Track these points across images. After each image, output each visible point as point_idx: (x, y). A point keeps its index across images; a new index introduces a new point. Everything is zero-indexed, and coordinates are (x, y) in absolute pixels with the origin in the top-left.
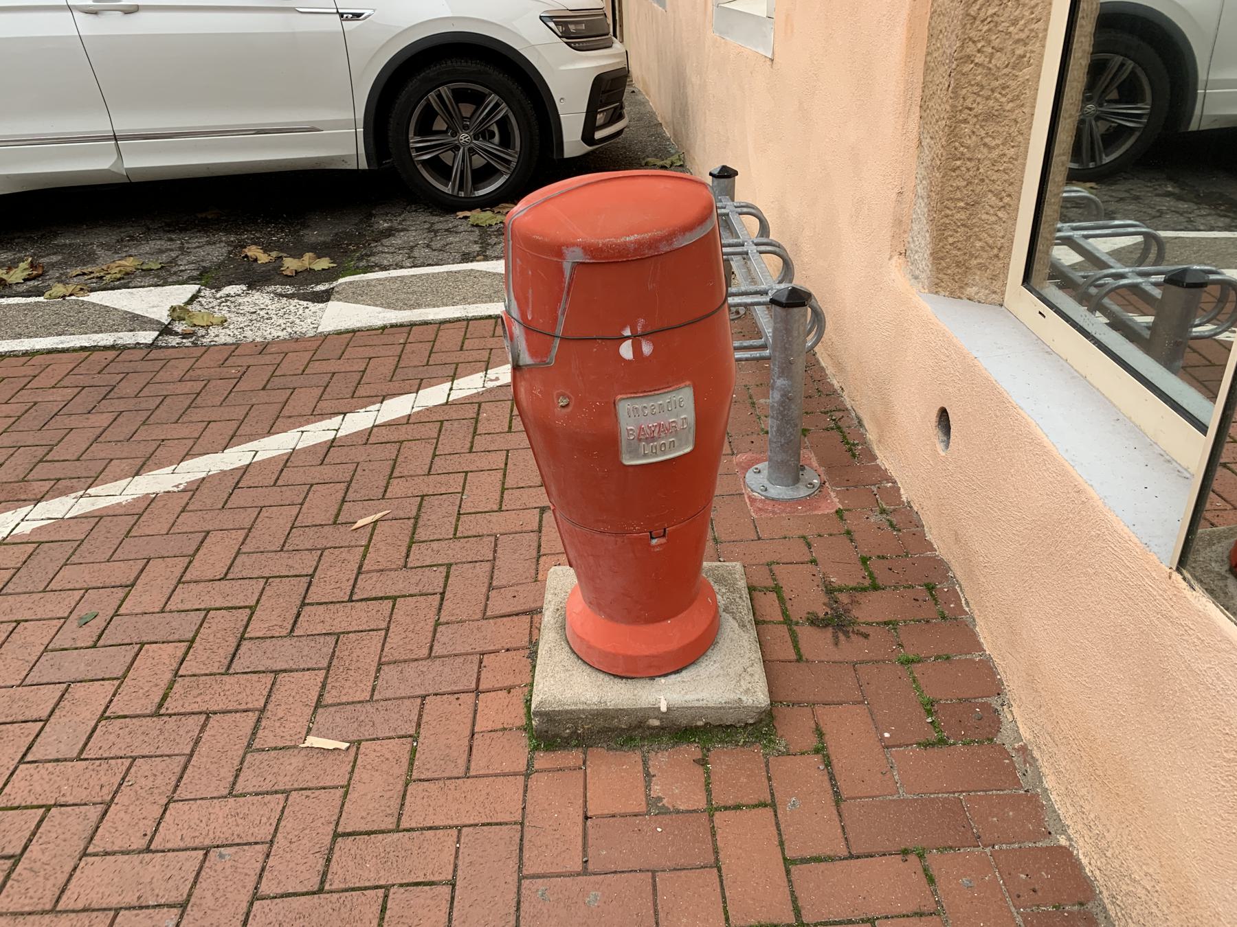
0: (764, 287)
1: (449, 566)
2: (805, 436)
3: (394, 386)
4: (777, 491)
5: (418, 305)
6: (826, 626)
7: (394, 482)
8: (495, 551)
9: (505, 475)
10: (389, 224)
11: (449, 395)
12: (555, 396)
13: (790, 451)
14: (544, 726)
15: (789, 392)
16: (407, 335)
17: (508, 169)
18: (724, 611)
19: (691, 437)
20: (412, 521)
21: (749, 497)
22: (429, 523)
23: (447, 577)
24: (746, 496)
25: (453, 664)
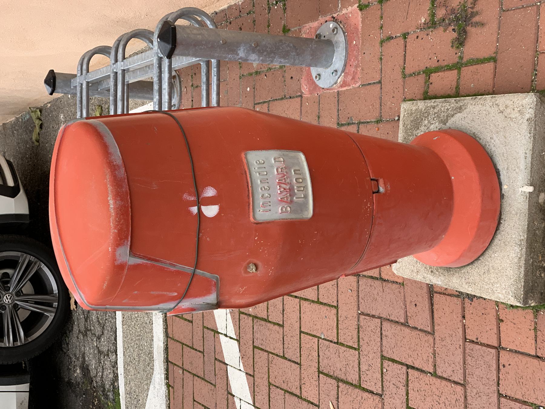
0: (155, 61)
1: (383, 358)
2: (289, 30)
3: (220, 383)
4: (338, 61)
5: (150, 354)
6: (465, 32)
7: (304, 395)
8: (373, 316)
9: (306, 300)
10: (78, 368)
11: (231, 338)
12: (246, 275)
13: (303, 48)
14: (537, 296)
15: (251, 45)
16: (175, 367)
17: (35, 263)
18: (445, 124)
19: (292, 154)
20: (340, 384)
21: (342, 86)
22: (343, 370)
23: (393, 361)
24: (341, 89)
25: (472, 366)
